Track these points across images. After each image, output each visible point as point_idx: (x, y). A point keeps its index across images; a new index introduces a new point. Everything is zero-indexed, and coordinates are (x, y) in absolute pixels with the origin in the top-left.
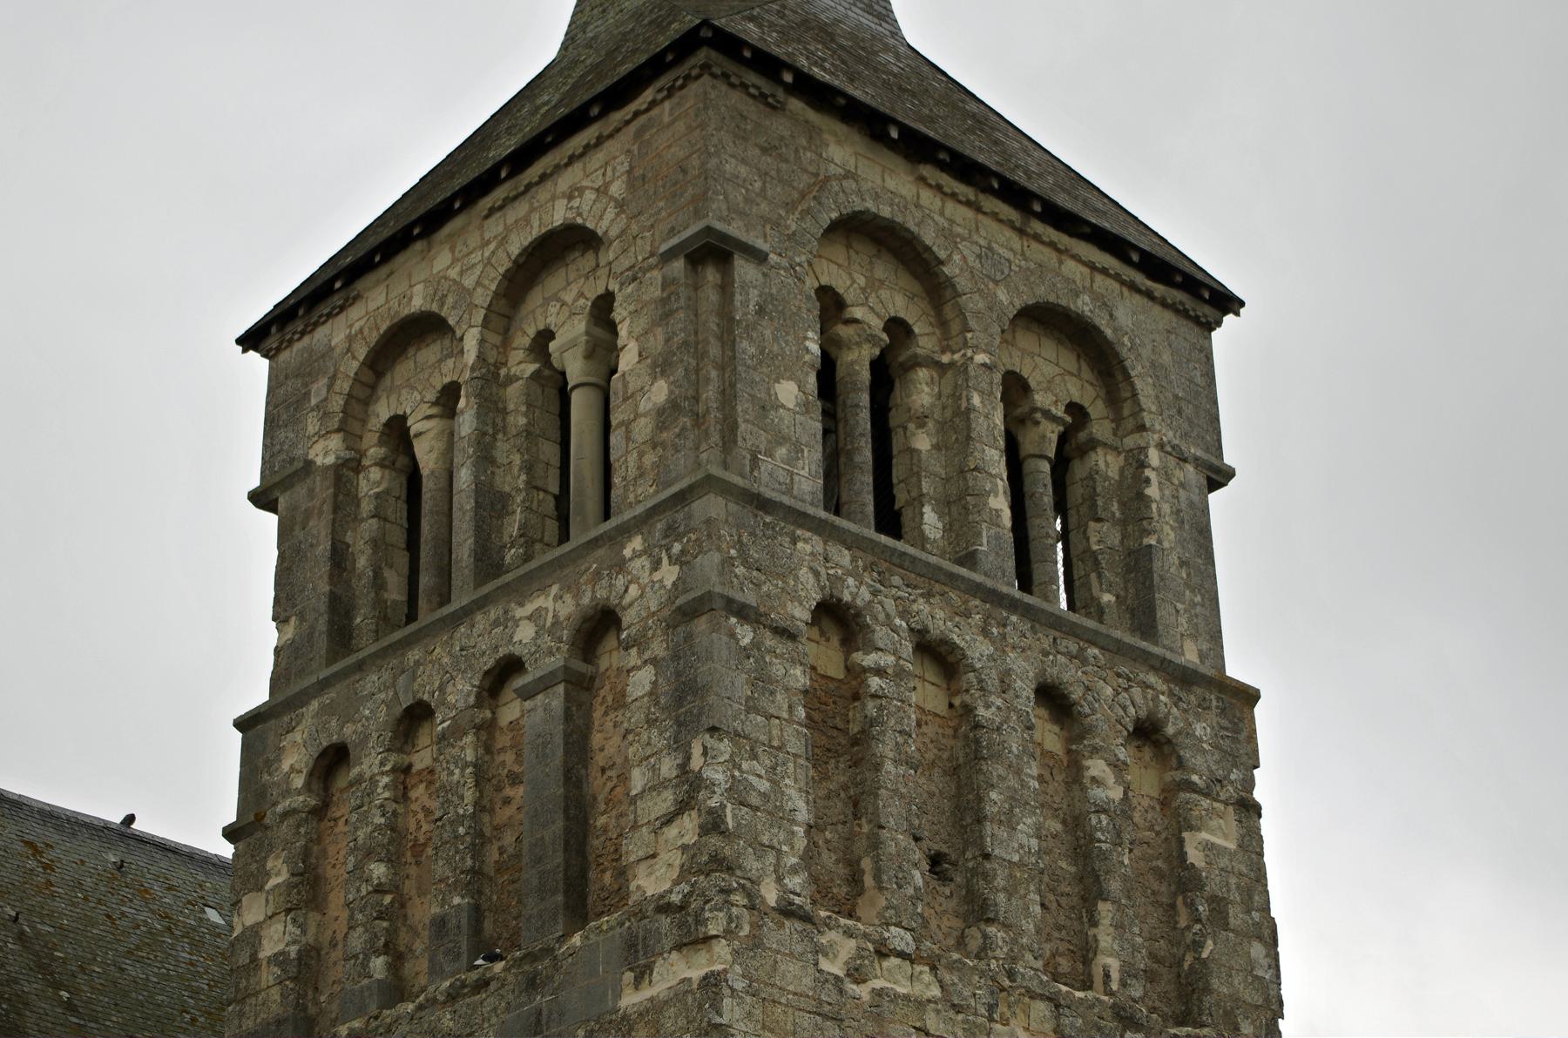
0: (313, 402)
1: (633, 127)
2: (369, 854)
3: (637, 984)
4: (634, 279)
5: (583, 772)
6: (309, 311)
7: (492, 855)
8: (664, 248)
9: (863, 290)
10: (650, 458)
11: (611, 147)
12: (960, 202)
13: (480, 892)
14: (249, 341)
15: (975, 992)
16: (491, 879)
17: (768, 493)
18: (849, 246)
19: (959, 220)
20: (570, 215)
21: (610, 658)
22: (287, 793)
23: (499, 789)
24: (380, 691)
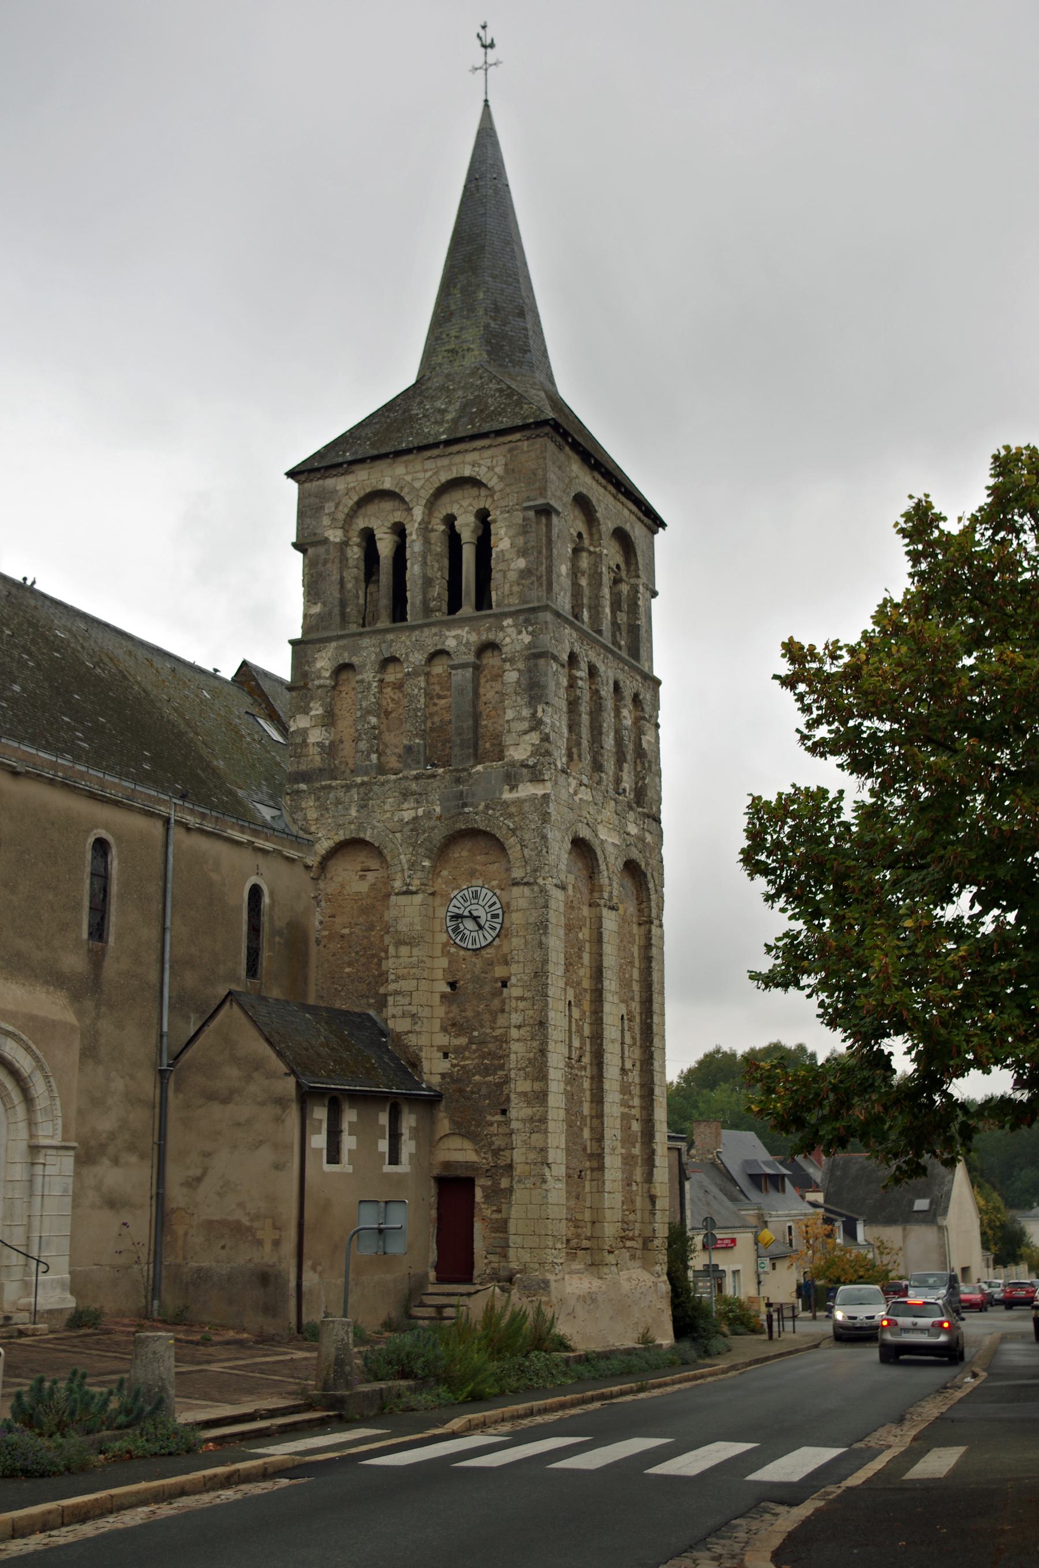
1: (508, 446)
2: (369, 712)
3: (511, 790)
8: (525, 505)
14: (292, 474)
15: (600, 799)
20: (474, 474)
21: (491, 660)
22: (319, 677)
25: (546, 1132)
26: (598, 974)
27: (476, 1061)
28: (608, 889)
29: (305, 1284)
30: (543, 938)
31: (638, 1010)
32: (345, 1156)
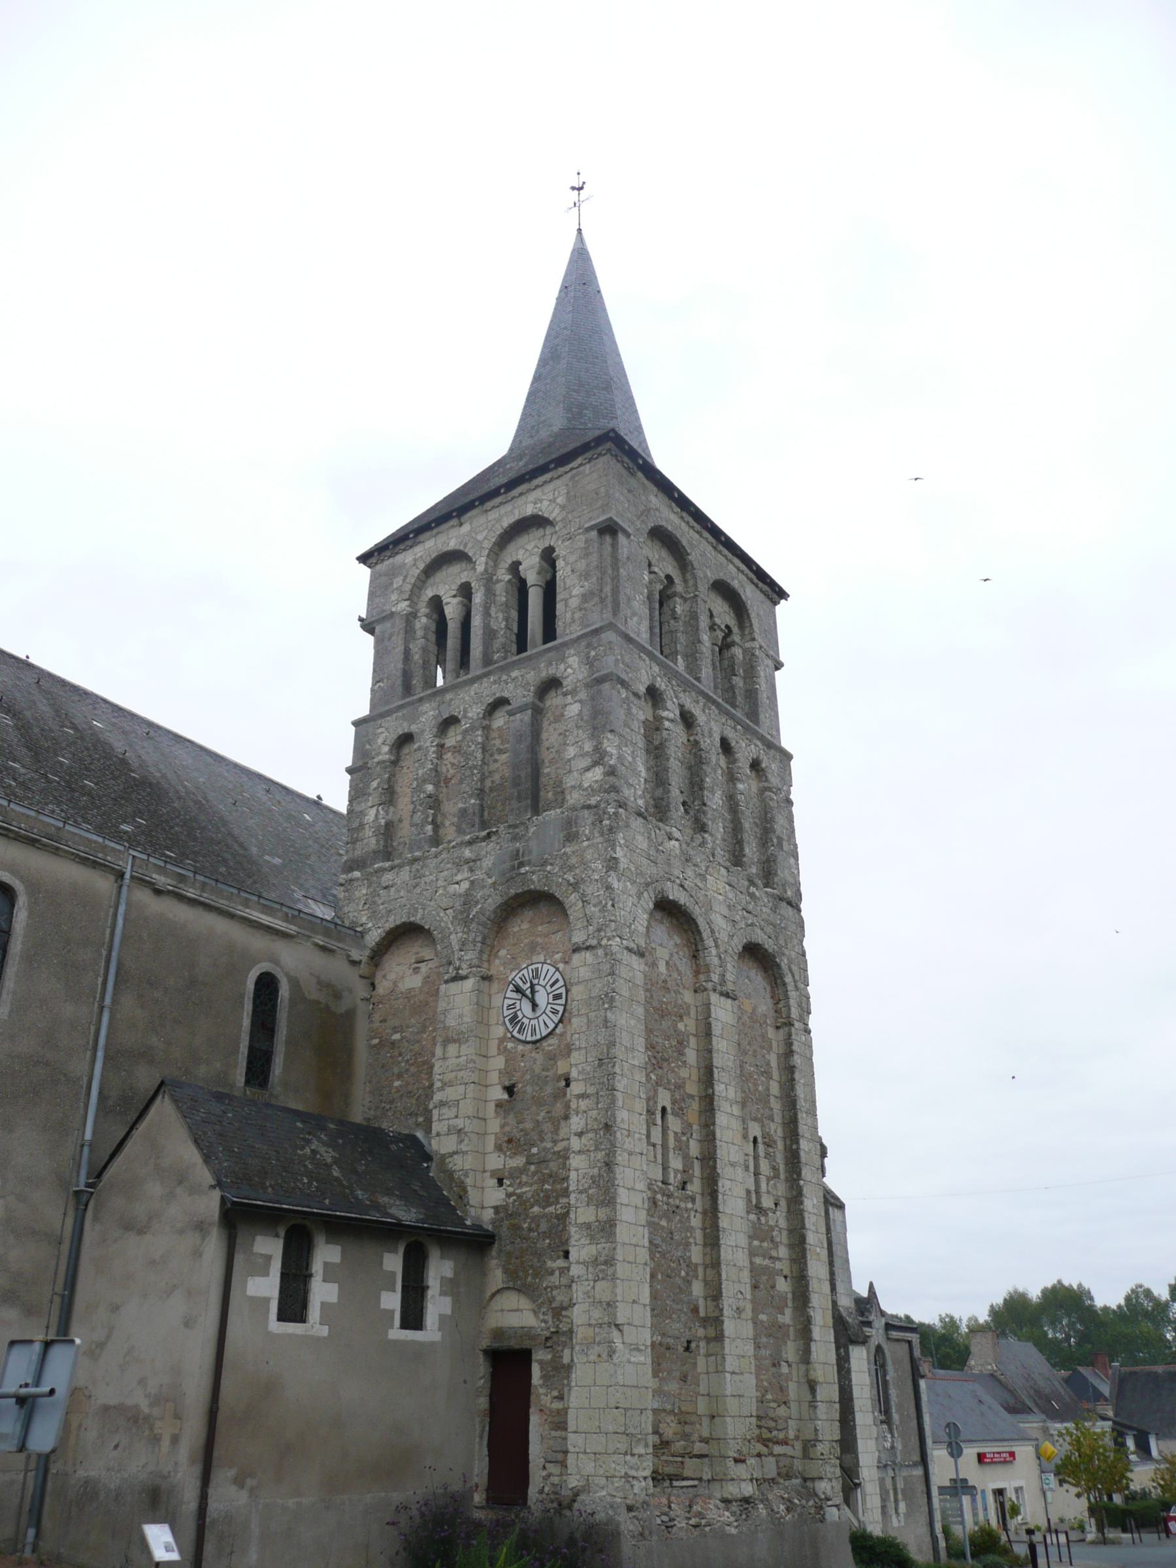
1: (569, 475)
2: (425, 781)
7: (488, 783)
8: (586, 526)
10: (577, 616)
11: (557, 482)
14: (364, 559)
17: (632, 635)
21: (554, 700)
22: (379, 754)
23: (492, 755)
25: (614, 1278)
26: (708, 1075)
27: (535, 1187)
28: (718, 970)
29: (215, 1507)
30: (609, 1014)
31: (780, 1132)
32: (314, 1312)
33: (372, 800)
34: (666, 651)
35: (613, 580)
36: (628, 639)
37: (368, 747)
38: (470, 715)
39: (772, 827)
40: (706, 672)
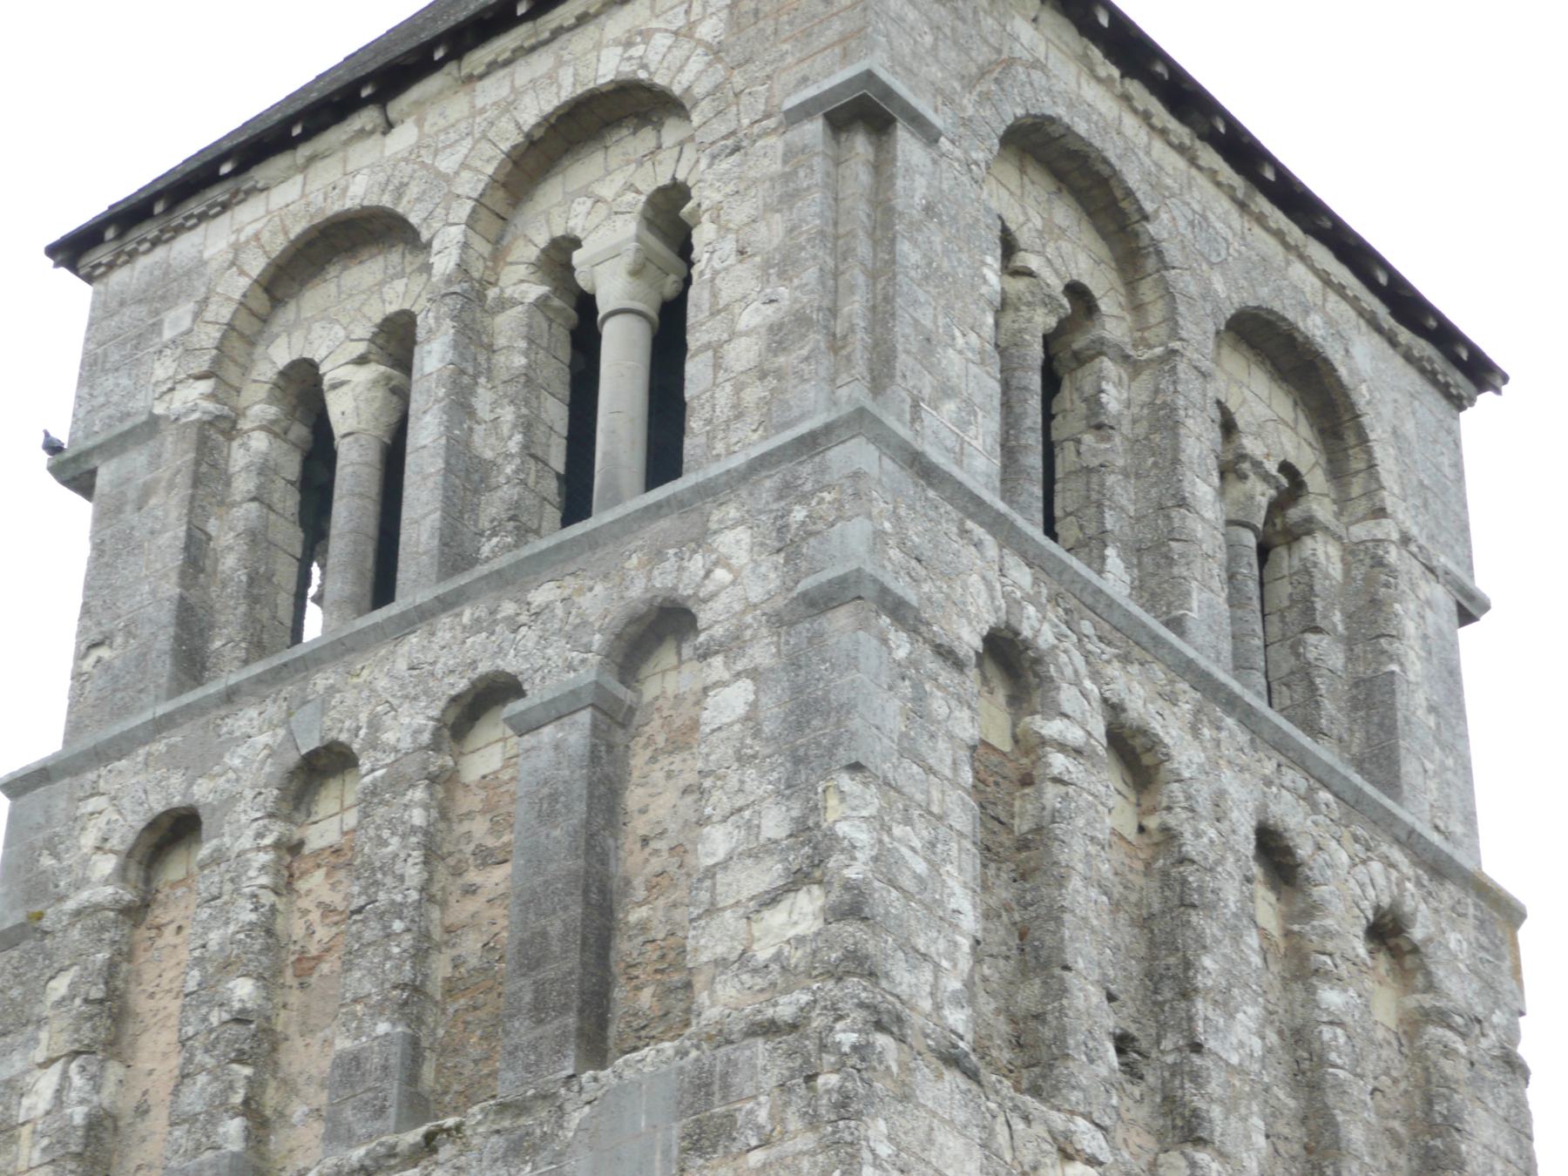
0: (168, 334)
2: (227, 967)
4: (737, 149)
5: (611, 842)
6: (169, 210)
7: (441, 967)
9: (1040, 233)
10: (754, 393)
12: (1170, 144)
13: (420, 1020)
16: (436, 1003)
18: (1022, 171)
19: (1169, 170)
20: (626, 68)
21: (669, 678)
23: (457, 872)
24: (261, 732)
33: (48, 1040)
34: (1065, 527)
35: (873, 276)
36: (924, 470)
37: (47, 861)
38: (389, 737)
39: (1452, 1151)
40: (1205, 603)
